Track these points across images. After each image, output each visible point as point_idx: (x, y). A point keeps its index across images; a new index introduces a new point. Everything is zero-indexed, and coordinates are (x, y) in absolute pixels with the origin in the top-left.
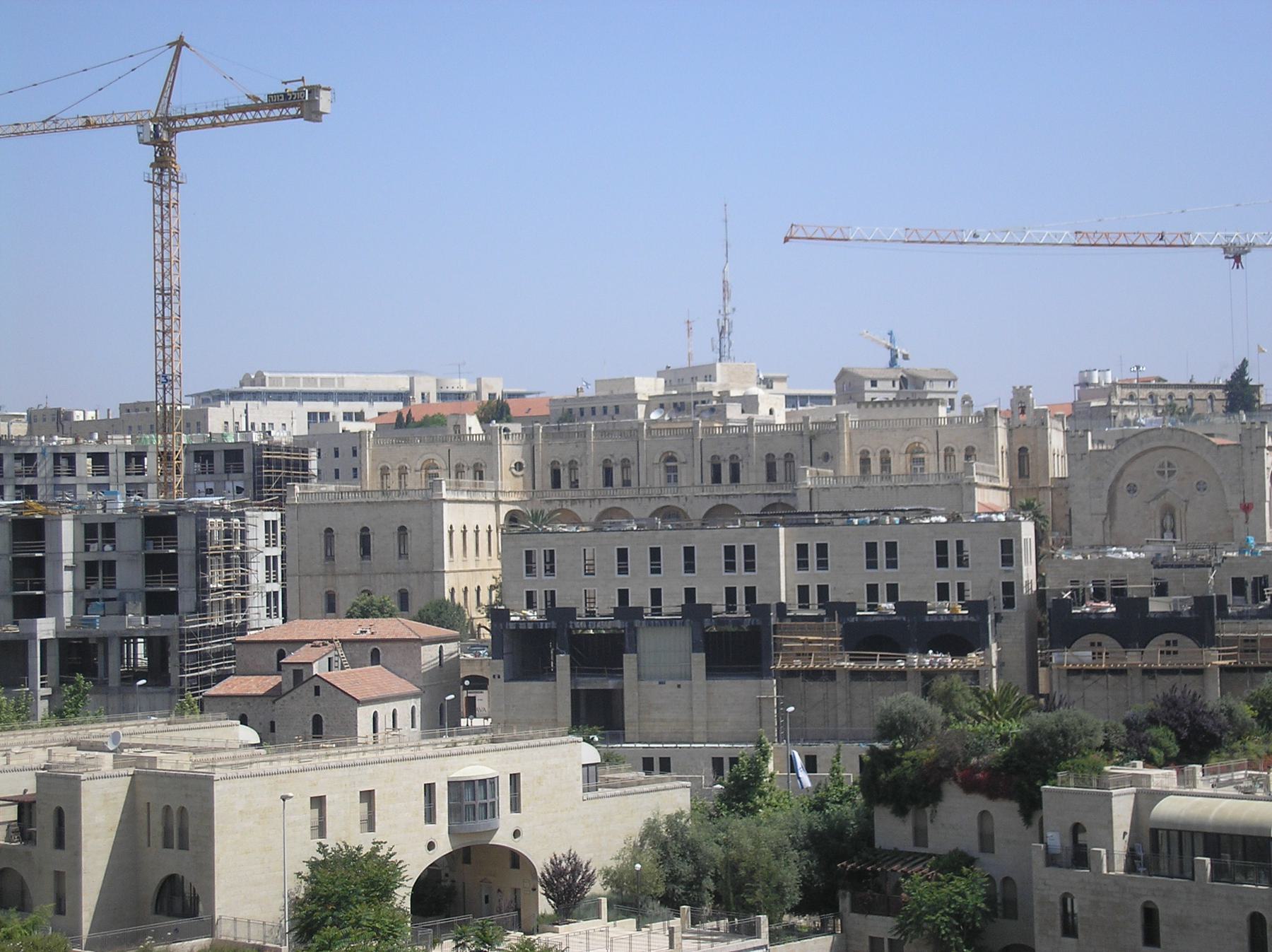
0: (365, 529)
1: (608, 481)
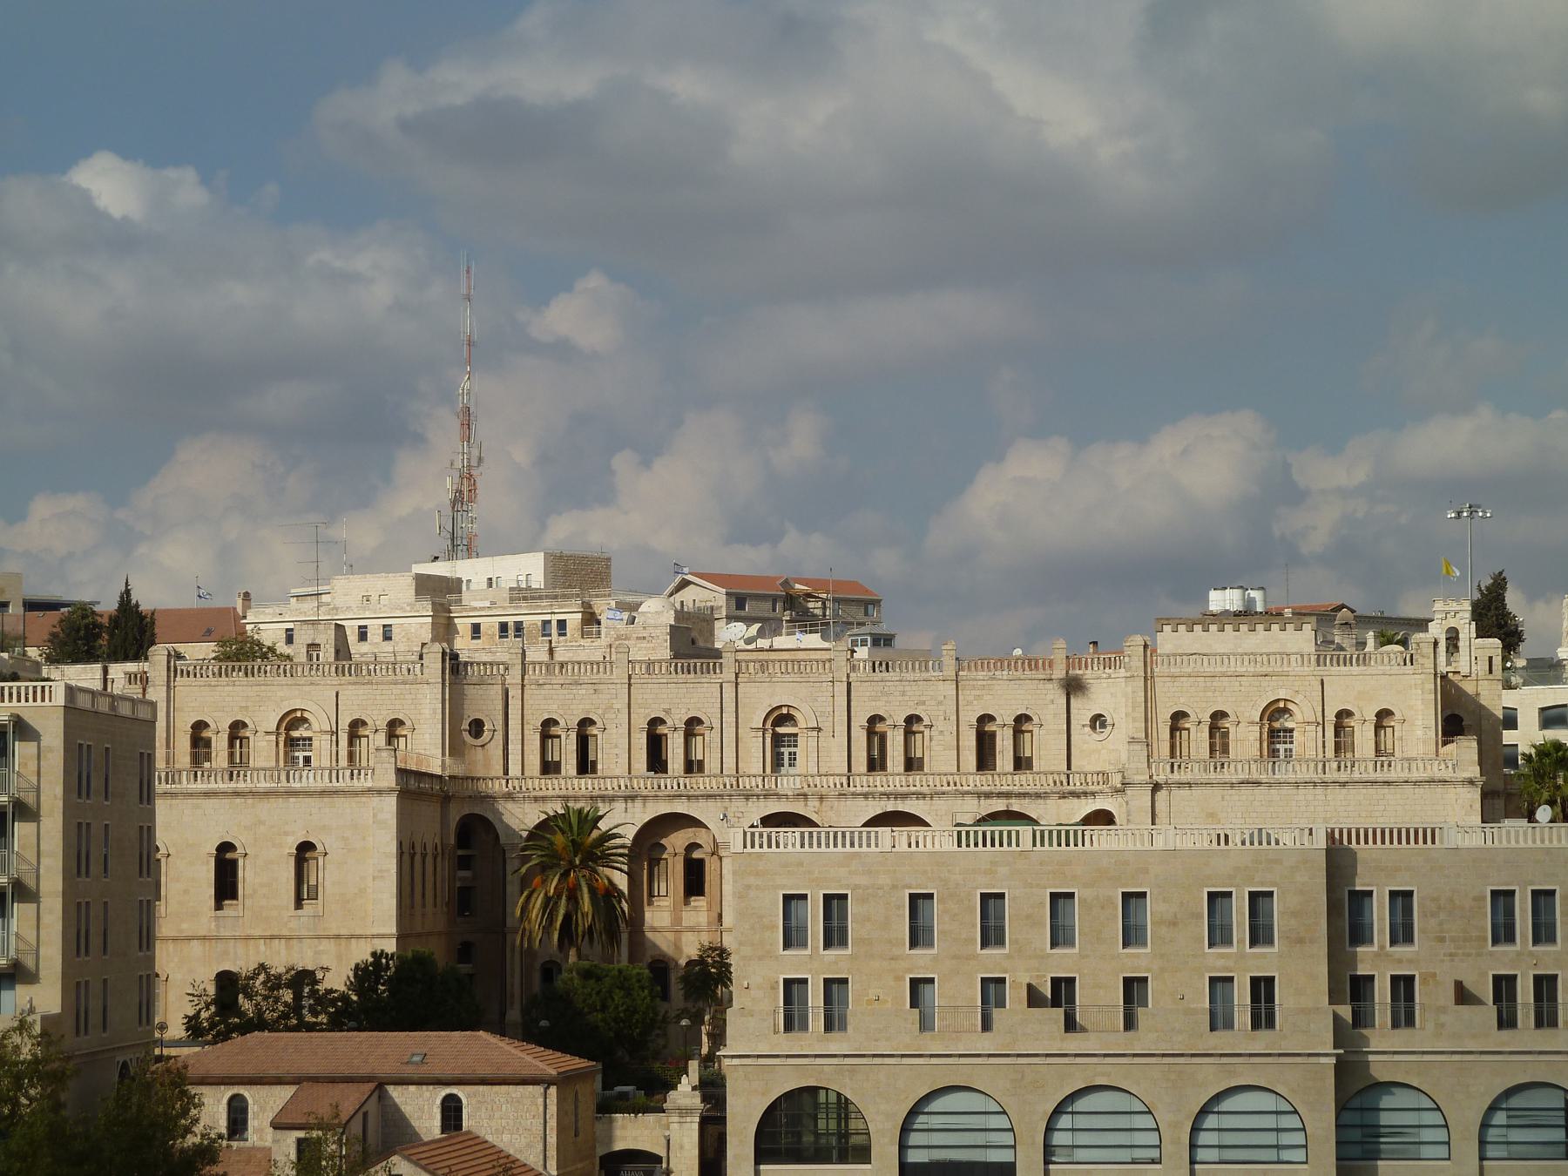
0: (226, 847)
1: (657, 762)
